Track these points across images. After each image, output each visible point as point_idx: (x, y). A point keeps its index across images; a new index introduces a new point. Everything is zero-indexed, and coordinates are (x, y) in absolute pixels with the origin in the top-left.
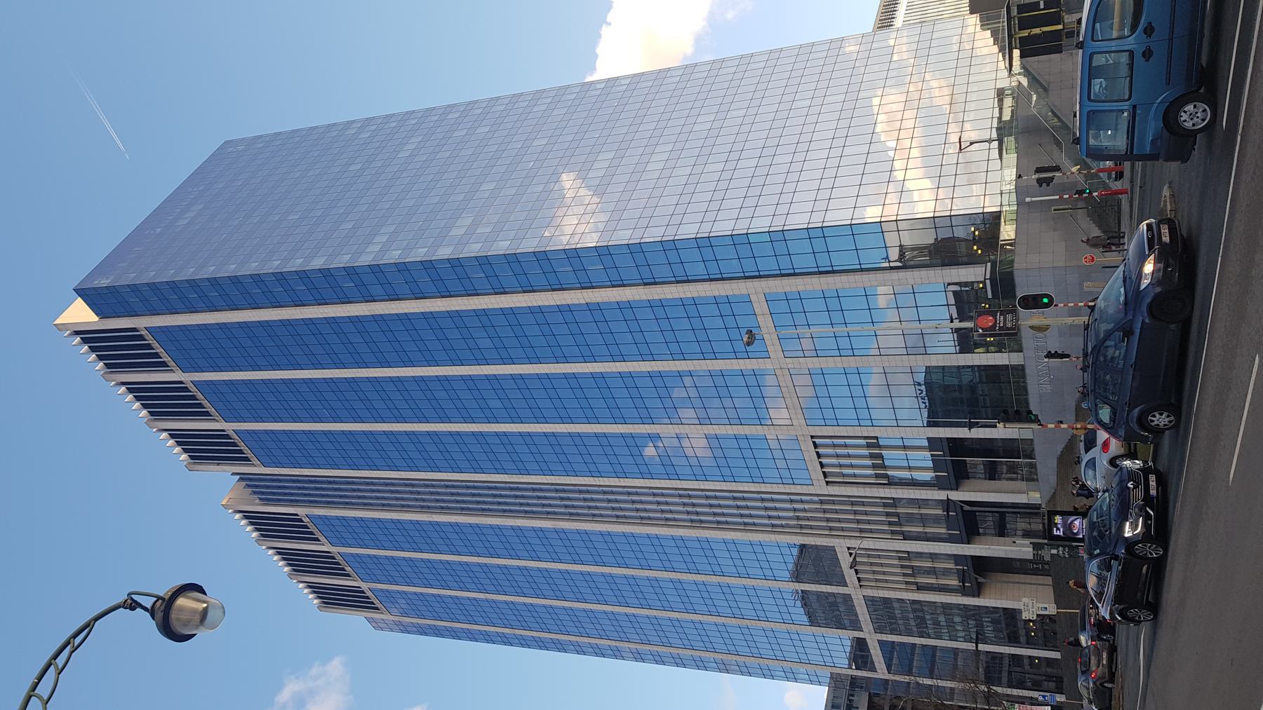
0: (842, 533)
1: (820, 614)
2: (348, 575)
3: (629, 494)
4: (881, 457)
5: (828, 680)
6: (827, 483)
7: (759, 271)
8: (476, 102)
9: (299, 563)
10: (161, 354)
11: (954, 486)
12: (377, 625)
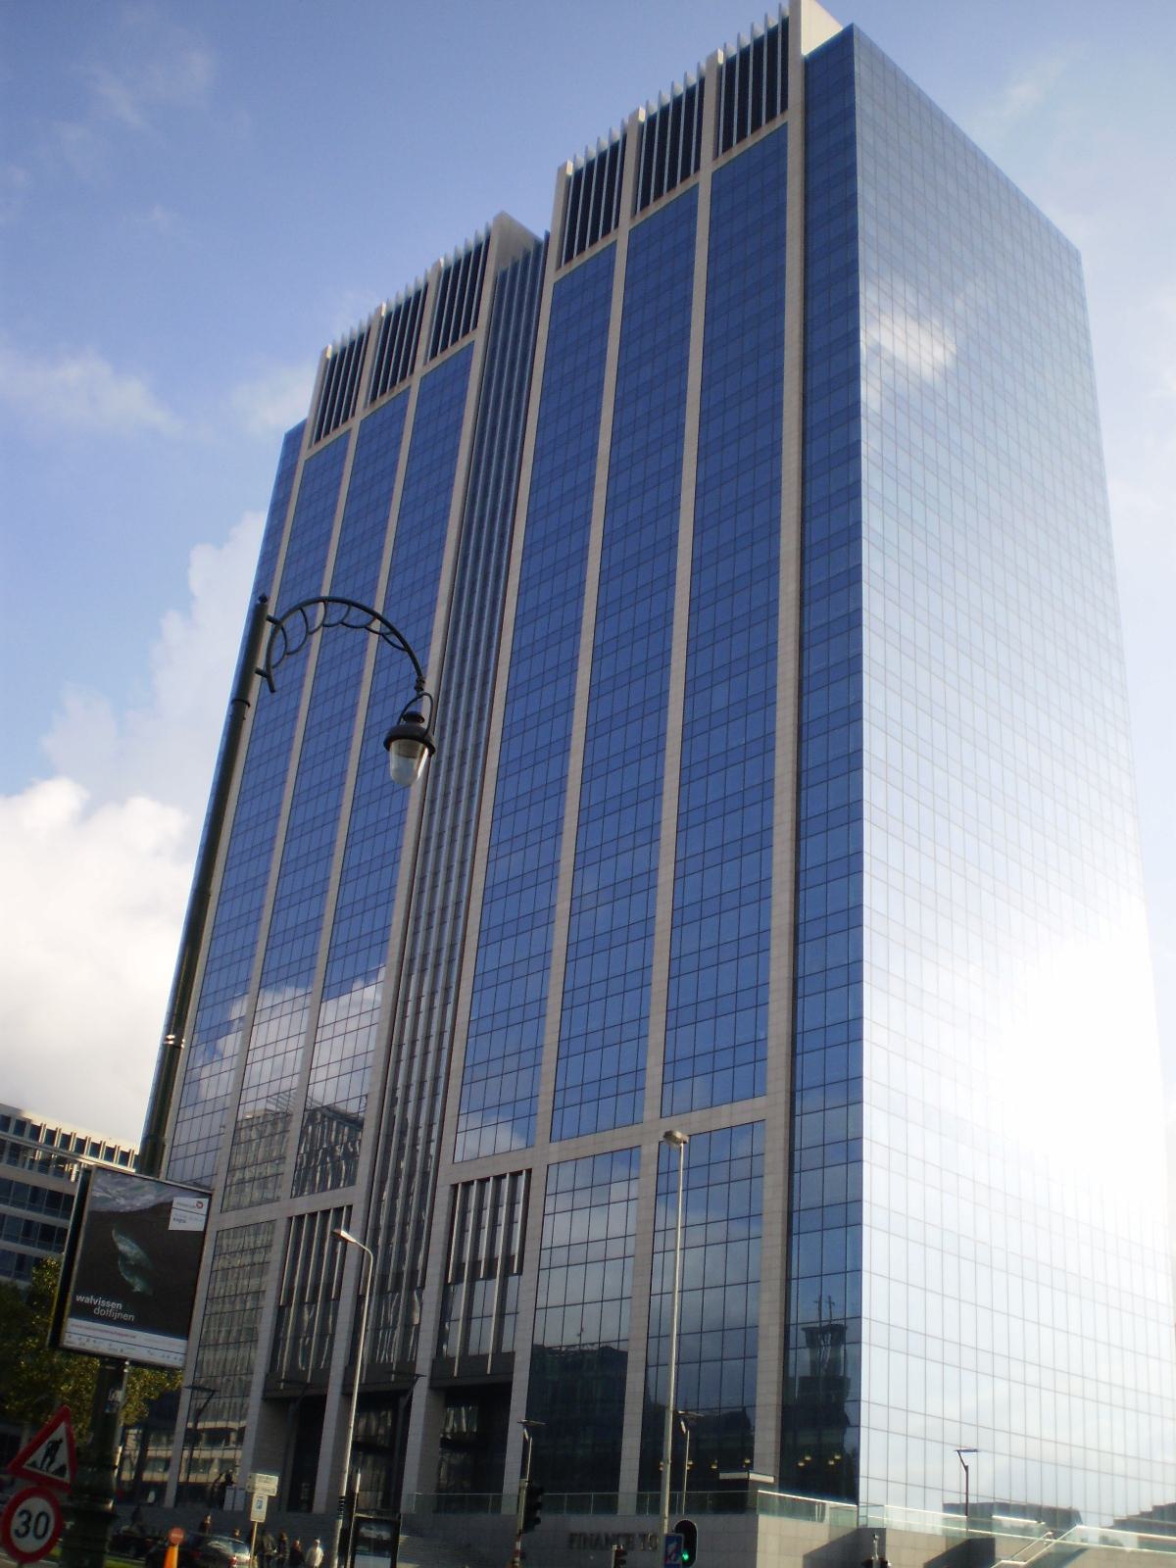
0: (373, 1199)
2: (374, 398)
3: (462, 863)
4: (490, 1274)
8: (1084, 307)
9: (401, 322)
12: (293, 439)
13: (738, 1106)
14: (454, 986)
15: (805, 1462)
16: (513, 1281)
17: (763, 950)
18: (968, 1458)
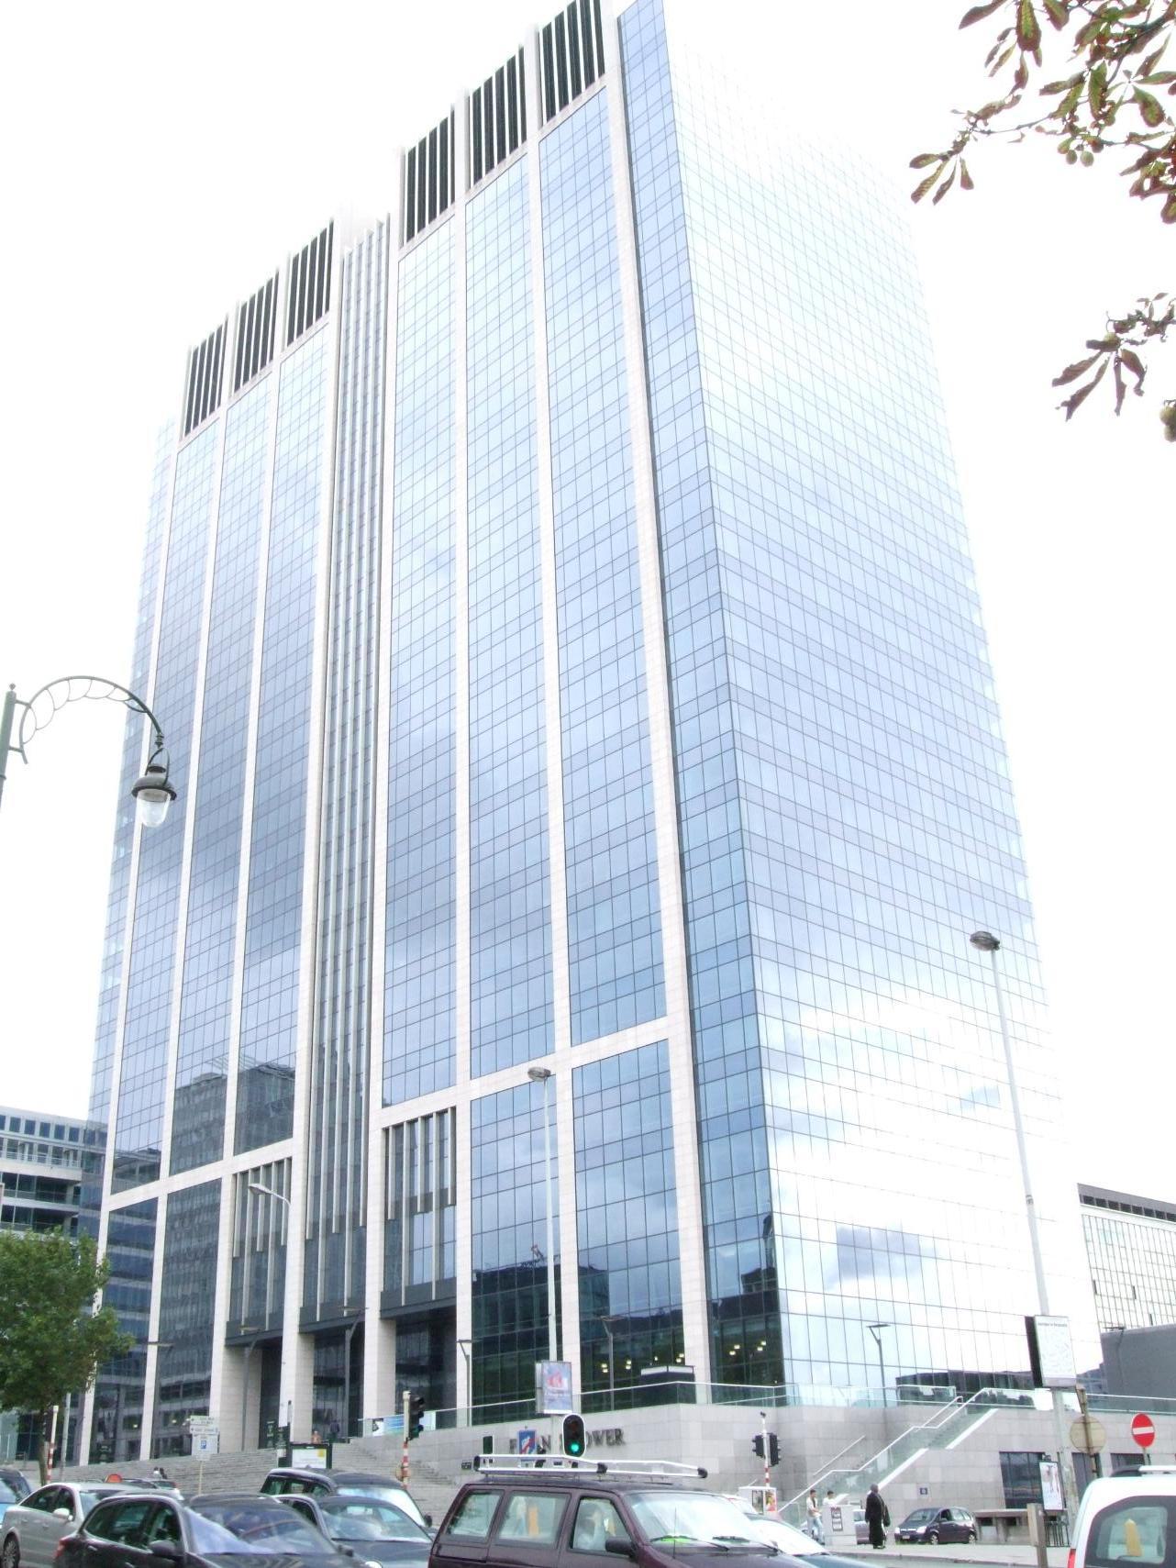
1: (178, 1312)
4: (427, 1208)
5: (96, 1119)
6: (386, 1130)
7: (715, 1247)
11: (387, 1314)
13: (642, 1028)
14: (367, 942)
15: (736, 1351)
16: (448, 1211)
17: (652, 881)
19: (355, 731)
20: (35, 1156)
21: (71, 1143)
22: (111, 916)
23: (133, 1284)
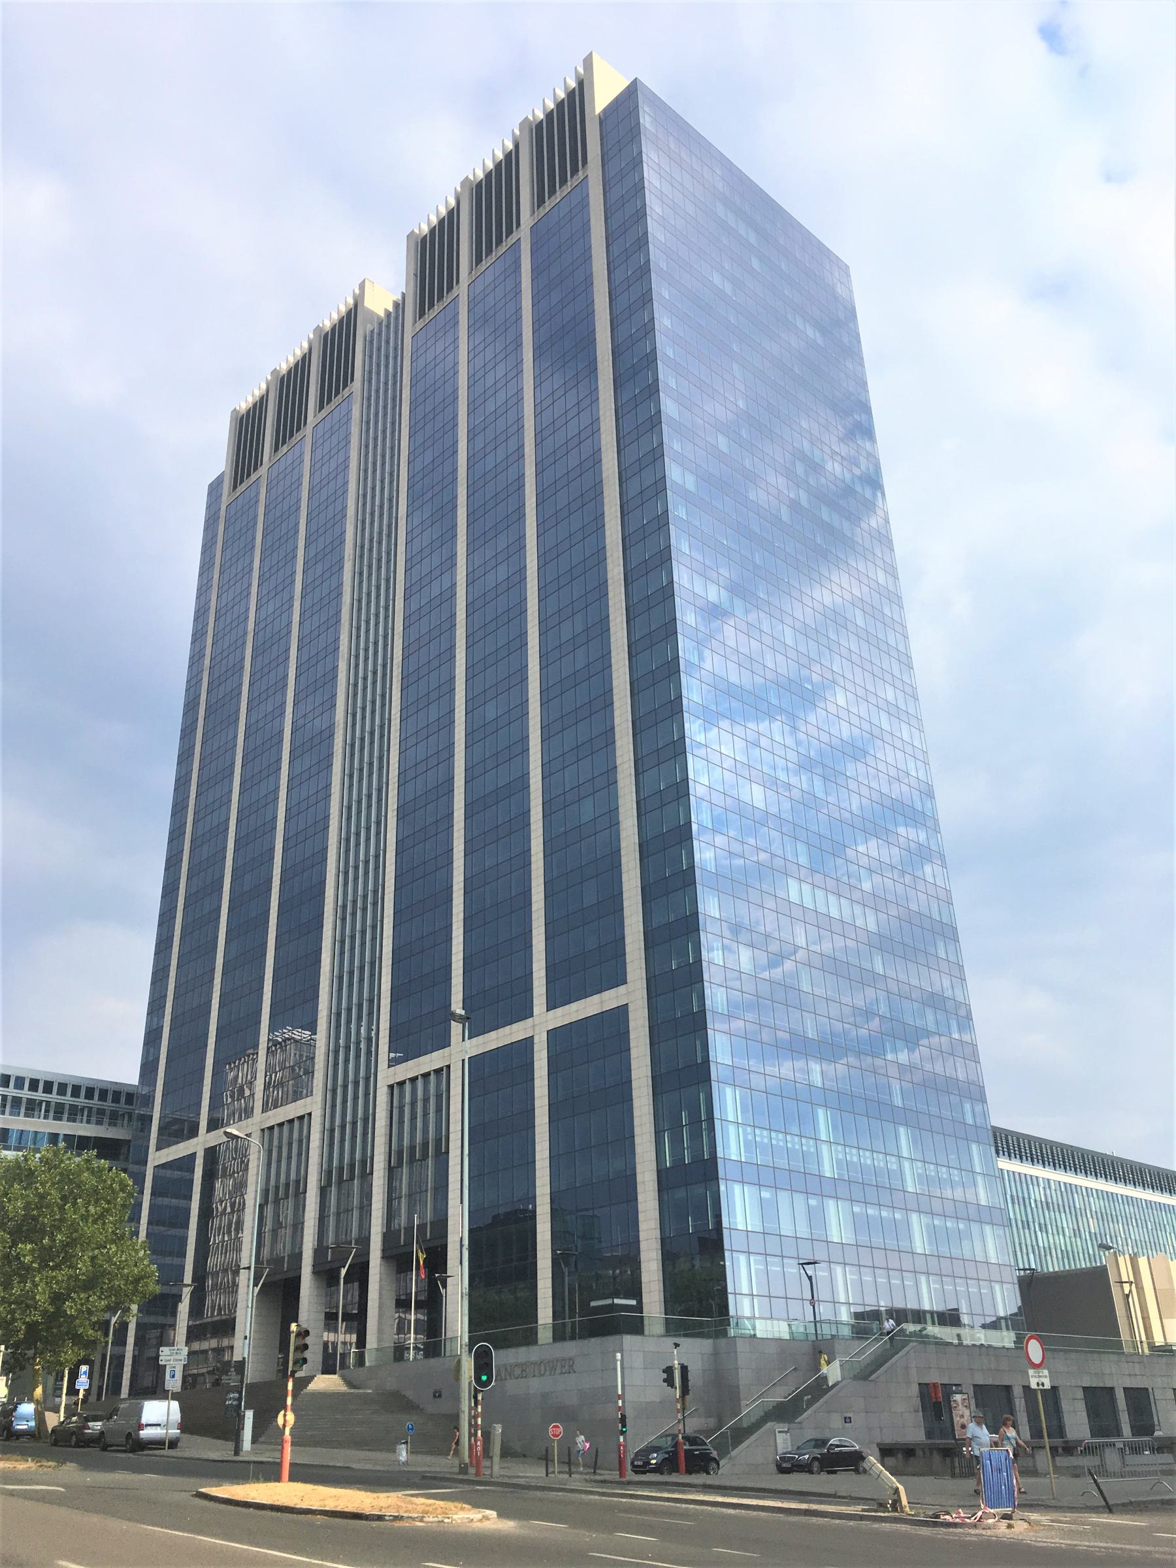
2: (276, 449)
7: (656, 996)
10: (564, 187)
12: (215, 489)
18: (810, 1269)
19: (373, 712)
20: (94, 1119)
21: (127, 1106)
22: (153, 995)
23: (173, 1232)
